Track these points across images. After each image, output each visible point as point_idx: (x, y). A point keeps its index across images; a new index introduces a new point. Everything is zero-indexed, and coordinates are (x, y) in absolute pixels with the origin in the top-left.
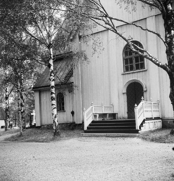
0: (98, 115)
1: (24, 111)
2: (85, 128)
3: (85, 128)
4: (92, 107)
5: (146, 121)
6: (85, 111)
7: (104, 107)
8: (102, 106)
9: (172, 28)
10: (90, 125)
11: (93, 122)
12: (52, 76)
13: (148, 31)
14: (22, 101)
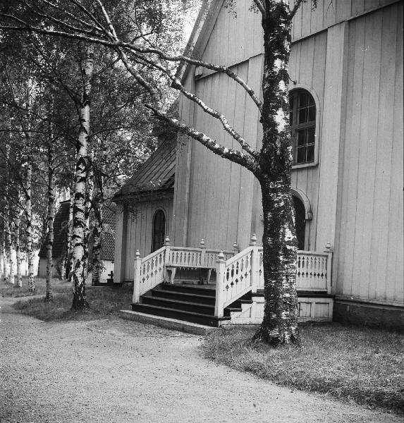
0: (174, 271)
1: (99, 246)
2: (136, 298)
3: (136, 298)
4: (252, 252)
5: (254, 299)
6: (138, 258)
7: (207, 252)
8: (200, 250)
9: (276, 54)
10: (153, 292)
11: (163, 285)
12: (80, 171)
13: (207, 69)
14: (98, 224)
